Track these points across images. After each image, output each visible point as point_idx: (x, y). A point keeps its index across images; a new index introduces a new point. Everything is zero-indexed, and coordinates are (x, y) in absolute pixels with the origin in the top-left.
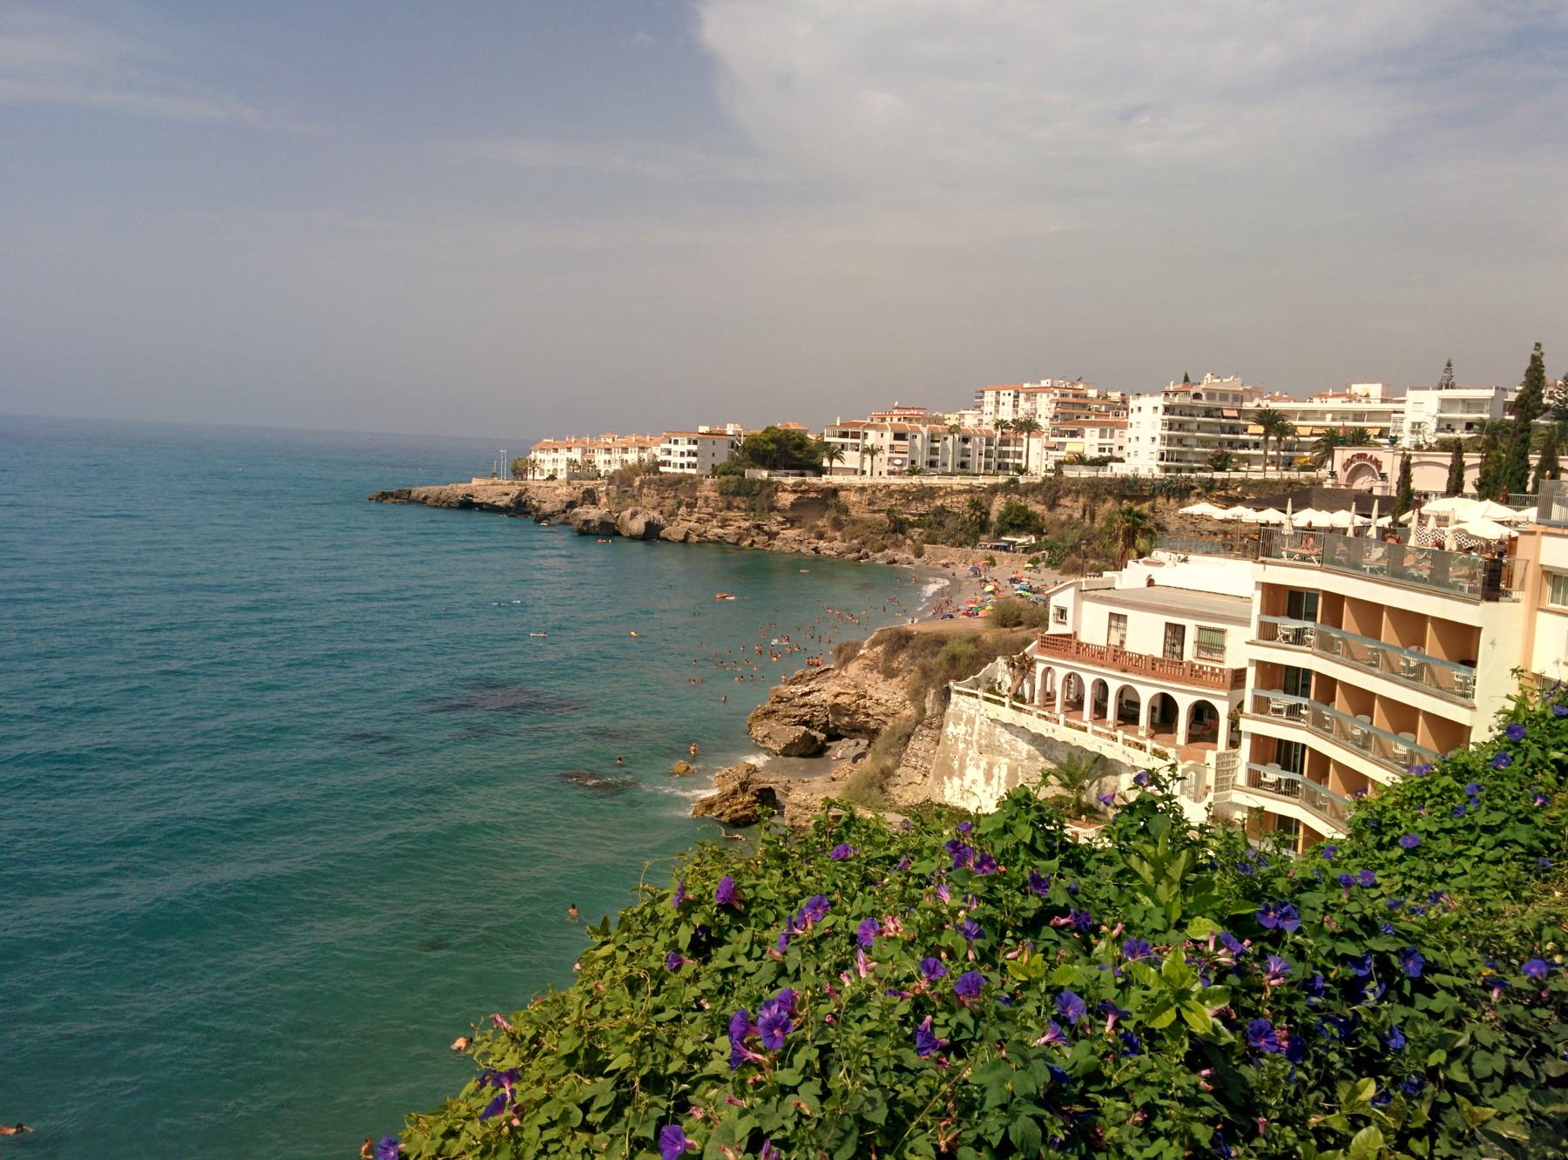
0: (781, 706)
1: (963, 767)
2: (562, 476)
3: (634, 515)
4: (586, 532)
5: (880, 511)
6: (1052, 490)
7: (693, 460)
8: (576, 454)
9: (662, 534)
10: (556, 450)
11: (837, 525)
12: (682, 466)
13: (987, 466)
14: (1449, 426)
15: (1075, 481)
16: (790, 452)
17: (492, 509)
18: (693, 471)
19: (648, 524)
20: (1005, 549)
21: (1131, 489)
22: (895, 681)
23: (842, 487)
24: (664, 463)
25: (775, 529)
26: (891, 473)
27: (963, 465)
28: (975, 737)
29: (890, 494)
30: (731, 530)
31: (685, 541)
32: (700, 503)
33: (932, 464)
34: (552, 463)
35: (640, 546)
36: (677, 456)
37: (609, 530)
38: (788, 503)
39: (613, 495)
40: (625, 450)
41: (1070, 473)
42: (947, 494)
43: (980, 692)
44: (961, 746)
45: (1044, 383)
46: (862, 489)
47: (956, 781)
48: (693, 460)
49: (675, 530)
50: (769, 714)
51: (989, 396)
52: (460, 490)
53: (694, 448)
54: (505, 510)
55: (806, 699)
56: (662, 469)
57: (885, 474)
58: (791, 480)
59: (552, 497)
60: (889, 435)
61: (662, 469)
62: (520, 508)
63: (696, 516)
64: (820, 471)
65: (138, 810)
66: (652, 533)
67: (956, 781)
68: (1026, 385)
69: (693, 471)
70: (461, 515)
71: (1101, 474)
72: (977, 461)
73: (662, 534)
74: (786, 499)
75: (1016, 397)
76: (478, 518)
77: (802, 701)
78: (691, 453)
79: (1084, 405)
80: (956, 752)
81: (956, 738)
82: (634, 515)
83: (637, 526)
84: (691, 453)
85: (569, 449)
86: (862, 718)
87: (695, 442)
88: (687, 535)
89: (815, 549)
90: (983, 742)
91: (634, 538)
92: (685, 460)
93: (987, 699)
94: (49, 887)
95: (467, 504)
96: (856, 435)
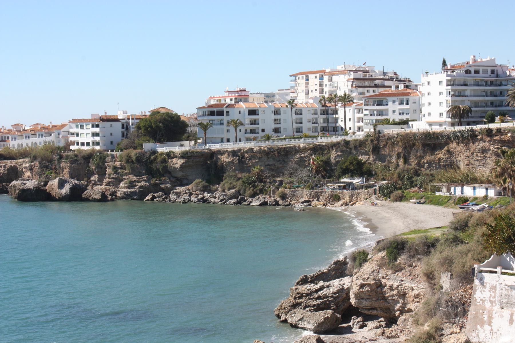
0: (302, 300)
1: (490, 317)
7: (97, 139)
9: (84, 195)
14: (501, 93)
18: (97, 148)
20: (344, 188)
21: (432, 142)
22: (400, 274)
23: (220, 152)
27: (299, 130)
28: (497, 299)
33: (277, 131)
35: (66, 206)
38: (178, 166)
39: (36, 169)
43: (498, 269)
44: (488, 305)
47: (487, 328)
48: (97, 139)
50: (294, 306)
53: (97, 130)
55: (320, 293)
56: (72, 147)
63: (106, 180)
67: (487, 328)
69: (97, 148)
71: (408, 130)
77: (316, 295)
78: (95, 135)
80: (484, 309)
81: (483, 301)
84: (95, 135)
87: (97, 126)
90: (504, 301)
93: (503, 273)
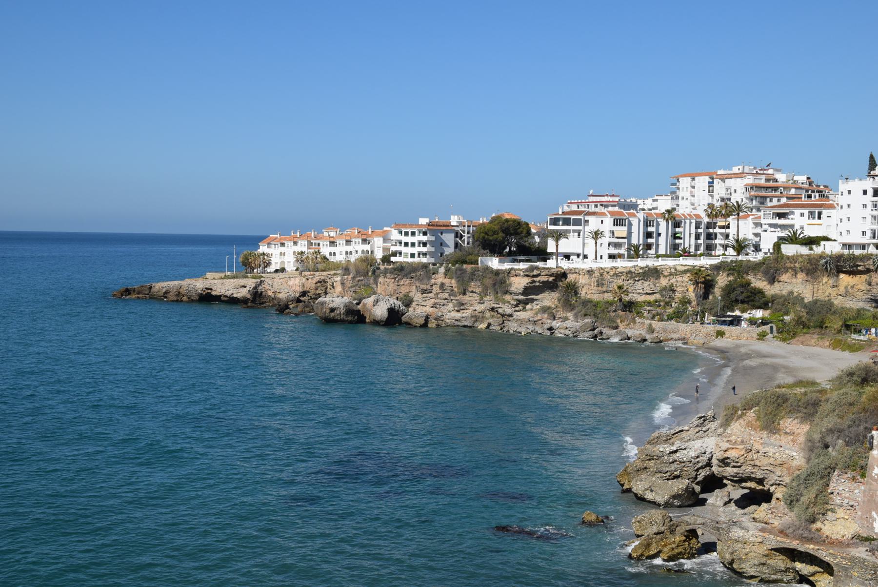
2: (290, 267)
3: (376, 302)
4: (330, 320)
5: (607, 292)
6: (774, 267)
8: (302, 246)
10: (283, 244)
11: (567, 305)
12: (413, 255)
13: (697, 247)
15: (793, 259)
16: (509, 238)
17: (232, 301)
19: (391, 311)
20: (731, 323)
24: (394, 254)
25: (508, 311)
26: (612, 257)
29: (617, 275)
30: (467, 313)
31: (425, 325)
32: (436, 289)
34: (282, 255)
35: (381, 332)
36: (411, 250)
37: (355, 317)
39: (349, 284)
40: (348, 242)
41: (789, 250)
42: (671, 274)
45: (735, 170)
46: (590, 272)
49: (417, 312)
51: (685, 182)
52: (199, 285)
54: (243, 302)
57: (605, 257)
58: (523, 266)
59: (286, 287)
60: (609, 221)
61: (393, 259)
62: (257, 299)
64: (544, 255)
65: (150, 565)
66: (394, 318)
68: (719, 172)
69: (424, 260)
70: (200, 309)
72: (688, 242)
73: (404, 319)
74: (519, 283)
75: (711, 184)
76: (216, 307)
79: (775, 189)
82: (376, 302)
83: (380, 311)
85: (295, 243)
86: (749, 469)
88: (427, 318)
89: (551, 329)
91: (376, 323)
92: (416, 250)
94: (551, 539)
95: (207, 298)
96: (577, 222)
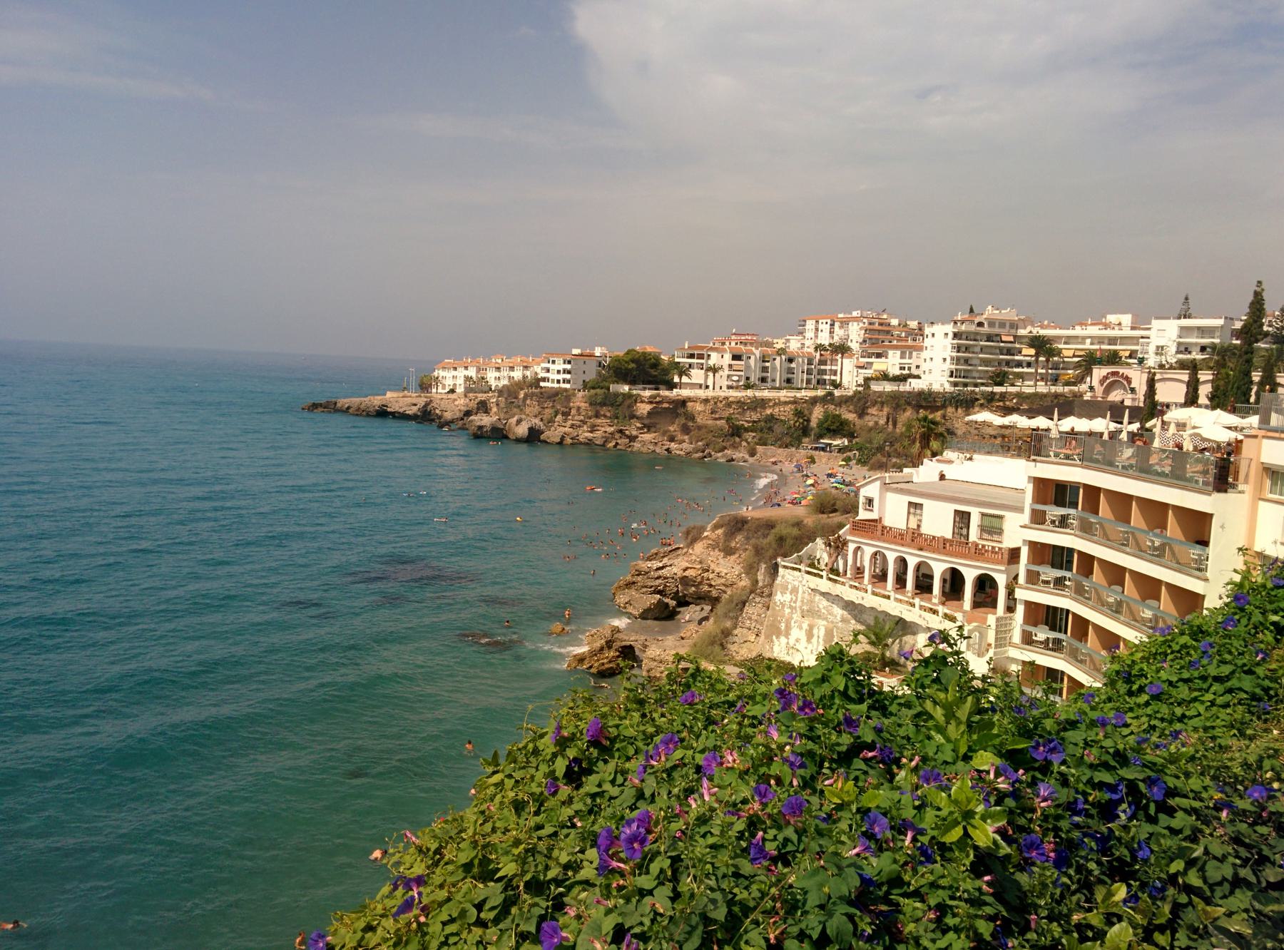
0: (639, 578)
1: (788, 628)
2: (460, 390)
3: (519, 422)
4: (480, 435)
5: (720, 419)
6: (862, 401)
7: (568, 376)
8: (472, 372)
9: (542, 437)
10: (455, 369)
11: (686, 430)
12: (558, 381)
13: (809, 381)
14: (1186, 349)
15: (881, 394)
16: (647, 370)
17: (403, 417)
18: (568, 386)
19: (531, 429)
20: (823, 449)
21: (926, 400)
22: (733, 558)
23: (690, 399)
24: (544, 379)
25: (634, 433)
26: (729, 387)
27: (789, 381)
28: (799, 604)
29: (729, 405)
30: (598, 434)
31: (561, 443)
32: (573, 412)
33: (763, 380)
34: (452, 379)
35: (524, 447)
36: (554, 374)
37: (499, 434)
38: (645, 412)
39: (502, 405)
40: (512, 369)
41: (876, 387)
42: (775, 404)
43: (802, 567)
44: (787, 611)
45: (855, 314)
46: (706, 401)
47: (783, 639)
48: (568, 376)
49: (553, 434)
50: (629, 585)
51: (810, 325)
52: (377, 401)
53: (568, 367)
54: (413, 418)
55: (660, 572)
56: (542, 384)
57: (724, 388)
58: (647, 393)
59: (452, 407)
60: (728, 357)
61: (542, 384)
62: (426, 416)
63: (570, 423)
64: (671, 386)
65: (113, 663)
66: (534, 437)
67: (783, 639)
68: (841, 316)
69: (568, 386)
70: (377, 422)
71: (902, 388)
72: (800, 378)
73: (542, 437)
74: (644, 409)
75: (832, 325)
76: (391, 425)
77: (657, 574)
78: (566, 371)
79: (888, 332)
80: (783, 616)
81: (783, 605)
82: (519, 422)
83: (522, 430)
84: (566, 371)
85: (466, 368)
86: (706, 588)
87: (569, 362)
88: (563, 438)
89: (668, 450)
90: (805, 608)
91: (519, 440)
92: (561, 377)
93: (808, 573)
95: (382, 413)
96: (701, 357)
